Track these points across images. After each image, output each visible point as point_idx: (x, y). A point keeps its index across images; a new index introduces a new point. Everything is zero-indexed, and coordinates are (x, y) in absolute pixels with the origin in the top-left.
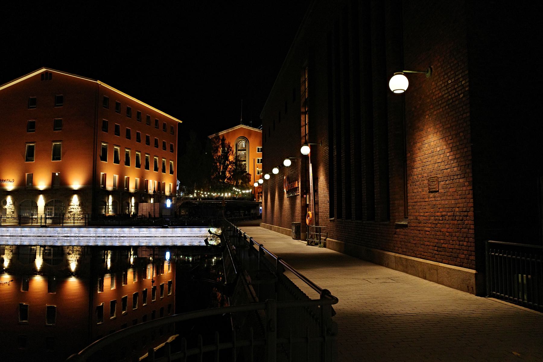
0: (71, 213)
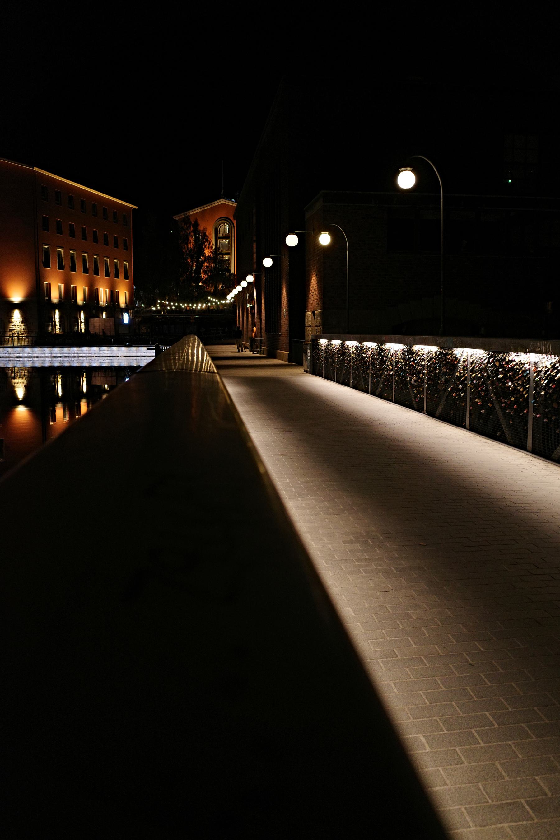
0: (13, 332)
